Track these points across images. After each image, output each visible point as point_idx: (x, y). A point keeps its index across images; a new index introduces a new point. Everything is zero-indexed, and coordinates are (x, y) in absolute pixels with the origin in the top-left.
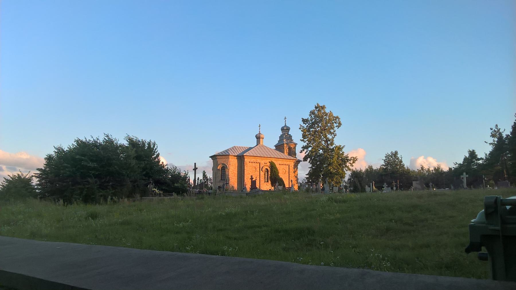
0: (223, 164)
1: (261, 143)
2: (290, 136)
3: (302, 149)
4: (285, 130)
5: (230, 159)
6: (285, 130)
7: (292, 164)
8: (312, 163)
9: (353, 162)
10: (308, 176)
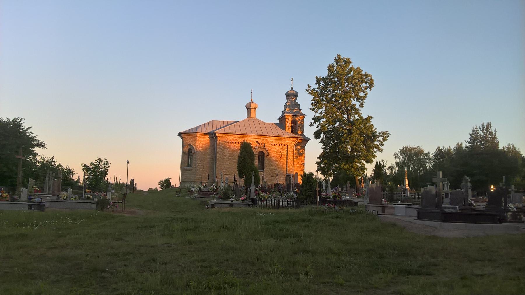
0: (190, 145)
1: (252, 115)
2: (298, 105)
3: (313, 121)
4: (292, 96)
5: (199, 139)
6: (292, 96)
7: (292, 144)
8: (325, 143)
9: (384, 140)
10: (319, 160)
